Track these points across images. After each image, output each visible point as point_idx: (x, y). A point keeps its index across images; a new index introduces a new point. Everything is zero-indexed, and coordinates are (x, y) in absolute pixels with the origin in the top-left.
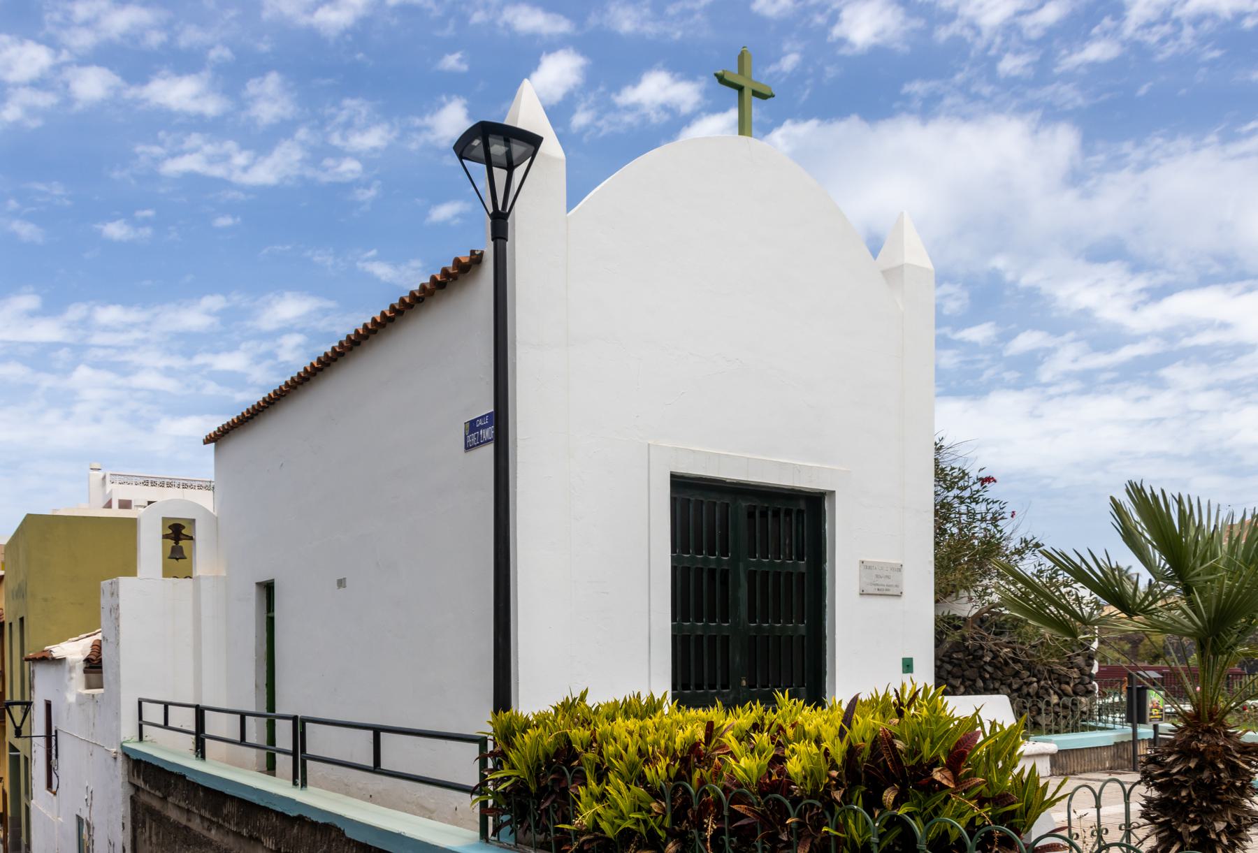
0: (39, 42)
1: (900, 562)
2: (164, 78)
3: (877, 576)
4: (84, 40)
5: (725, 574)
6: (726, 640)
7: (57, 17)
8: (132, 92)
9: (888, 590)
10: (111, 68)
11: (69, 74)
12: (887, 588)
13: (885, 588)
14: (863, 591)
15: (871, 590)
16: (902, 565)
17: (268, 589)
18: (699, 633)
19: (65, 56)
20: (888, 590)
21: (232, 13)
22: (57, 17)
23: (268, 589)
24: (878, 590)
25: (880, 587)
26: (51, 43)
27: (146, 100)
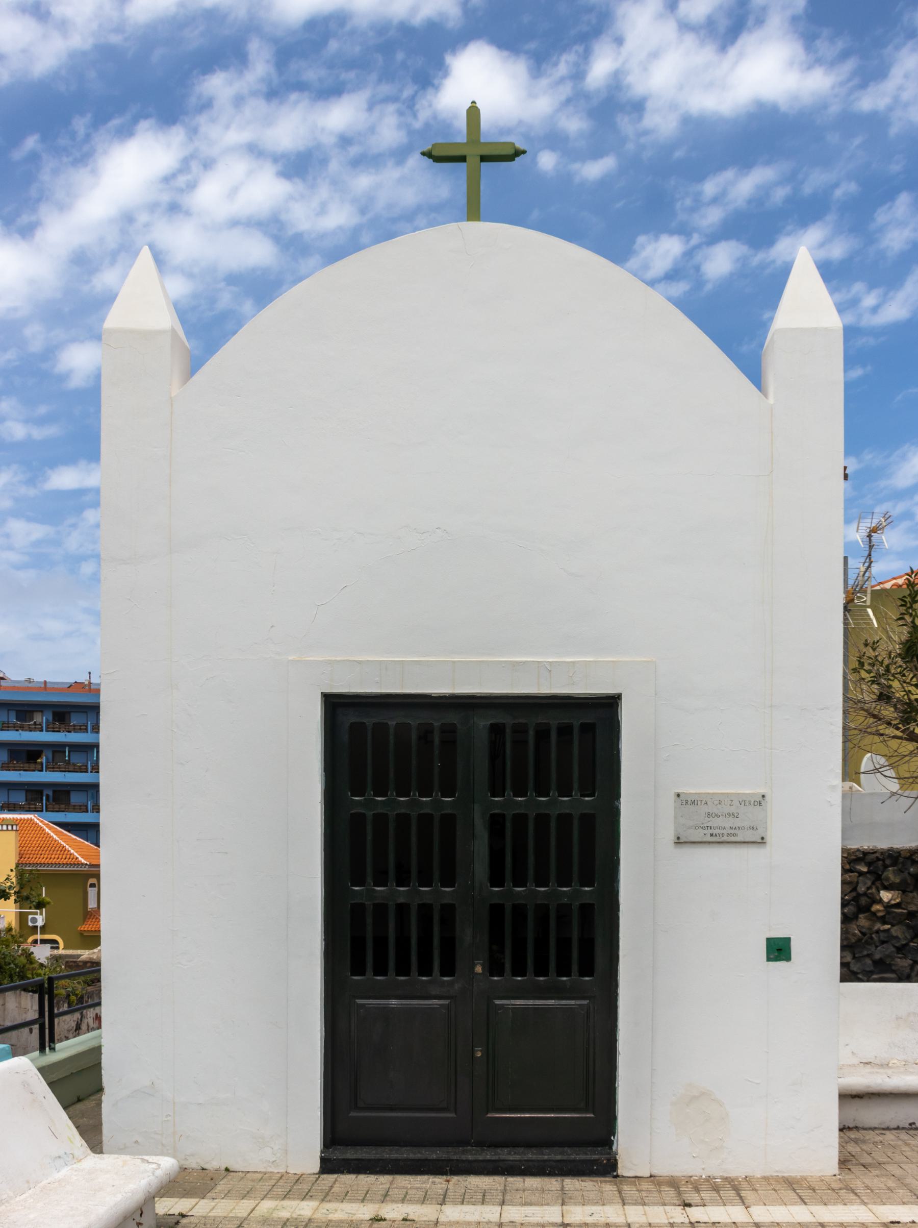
0: (672, 233)
1: (762, 791)
2: (789, 234)
3: (709, 815)
4: (713, 217)
5: (449, 821)
6: (448, 912)
7: (688, 202)
8: (759, 257)
9: (735, 835)
10: (738, 240)
11: (698, 257)
12: (732, 831)
13: (725, 832)
14: (678, 838)
15: (698, 835)
16: (763, 796)
17: (905, 812)
18: (401, 900)
19: (696, 239)
20: (735, 835)
21: (857, 141)
22: (688, 202)
23: (905, 812)
24: (712, 835)
25: (715, 832)
26: (684, 231)
27: (774, 262)
